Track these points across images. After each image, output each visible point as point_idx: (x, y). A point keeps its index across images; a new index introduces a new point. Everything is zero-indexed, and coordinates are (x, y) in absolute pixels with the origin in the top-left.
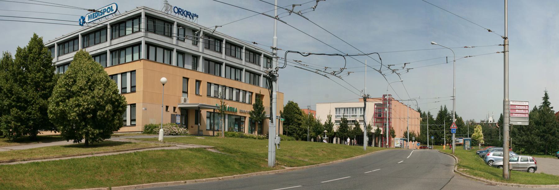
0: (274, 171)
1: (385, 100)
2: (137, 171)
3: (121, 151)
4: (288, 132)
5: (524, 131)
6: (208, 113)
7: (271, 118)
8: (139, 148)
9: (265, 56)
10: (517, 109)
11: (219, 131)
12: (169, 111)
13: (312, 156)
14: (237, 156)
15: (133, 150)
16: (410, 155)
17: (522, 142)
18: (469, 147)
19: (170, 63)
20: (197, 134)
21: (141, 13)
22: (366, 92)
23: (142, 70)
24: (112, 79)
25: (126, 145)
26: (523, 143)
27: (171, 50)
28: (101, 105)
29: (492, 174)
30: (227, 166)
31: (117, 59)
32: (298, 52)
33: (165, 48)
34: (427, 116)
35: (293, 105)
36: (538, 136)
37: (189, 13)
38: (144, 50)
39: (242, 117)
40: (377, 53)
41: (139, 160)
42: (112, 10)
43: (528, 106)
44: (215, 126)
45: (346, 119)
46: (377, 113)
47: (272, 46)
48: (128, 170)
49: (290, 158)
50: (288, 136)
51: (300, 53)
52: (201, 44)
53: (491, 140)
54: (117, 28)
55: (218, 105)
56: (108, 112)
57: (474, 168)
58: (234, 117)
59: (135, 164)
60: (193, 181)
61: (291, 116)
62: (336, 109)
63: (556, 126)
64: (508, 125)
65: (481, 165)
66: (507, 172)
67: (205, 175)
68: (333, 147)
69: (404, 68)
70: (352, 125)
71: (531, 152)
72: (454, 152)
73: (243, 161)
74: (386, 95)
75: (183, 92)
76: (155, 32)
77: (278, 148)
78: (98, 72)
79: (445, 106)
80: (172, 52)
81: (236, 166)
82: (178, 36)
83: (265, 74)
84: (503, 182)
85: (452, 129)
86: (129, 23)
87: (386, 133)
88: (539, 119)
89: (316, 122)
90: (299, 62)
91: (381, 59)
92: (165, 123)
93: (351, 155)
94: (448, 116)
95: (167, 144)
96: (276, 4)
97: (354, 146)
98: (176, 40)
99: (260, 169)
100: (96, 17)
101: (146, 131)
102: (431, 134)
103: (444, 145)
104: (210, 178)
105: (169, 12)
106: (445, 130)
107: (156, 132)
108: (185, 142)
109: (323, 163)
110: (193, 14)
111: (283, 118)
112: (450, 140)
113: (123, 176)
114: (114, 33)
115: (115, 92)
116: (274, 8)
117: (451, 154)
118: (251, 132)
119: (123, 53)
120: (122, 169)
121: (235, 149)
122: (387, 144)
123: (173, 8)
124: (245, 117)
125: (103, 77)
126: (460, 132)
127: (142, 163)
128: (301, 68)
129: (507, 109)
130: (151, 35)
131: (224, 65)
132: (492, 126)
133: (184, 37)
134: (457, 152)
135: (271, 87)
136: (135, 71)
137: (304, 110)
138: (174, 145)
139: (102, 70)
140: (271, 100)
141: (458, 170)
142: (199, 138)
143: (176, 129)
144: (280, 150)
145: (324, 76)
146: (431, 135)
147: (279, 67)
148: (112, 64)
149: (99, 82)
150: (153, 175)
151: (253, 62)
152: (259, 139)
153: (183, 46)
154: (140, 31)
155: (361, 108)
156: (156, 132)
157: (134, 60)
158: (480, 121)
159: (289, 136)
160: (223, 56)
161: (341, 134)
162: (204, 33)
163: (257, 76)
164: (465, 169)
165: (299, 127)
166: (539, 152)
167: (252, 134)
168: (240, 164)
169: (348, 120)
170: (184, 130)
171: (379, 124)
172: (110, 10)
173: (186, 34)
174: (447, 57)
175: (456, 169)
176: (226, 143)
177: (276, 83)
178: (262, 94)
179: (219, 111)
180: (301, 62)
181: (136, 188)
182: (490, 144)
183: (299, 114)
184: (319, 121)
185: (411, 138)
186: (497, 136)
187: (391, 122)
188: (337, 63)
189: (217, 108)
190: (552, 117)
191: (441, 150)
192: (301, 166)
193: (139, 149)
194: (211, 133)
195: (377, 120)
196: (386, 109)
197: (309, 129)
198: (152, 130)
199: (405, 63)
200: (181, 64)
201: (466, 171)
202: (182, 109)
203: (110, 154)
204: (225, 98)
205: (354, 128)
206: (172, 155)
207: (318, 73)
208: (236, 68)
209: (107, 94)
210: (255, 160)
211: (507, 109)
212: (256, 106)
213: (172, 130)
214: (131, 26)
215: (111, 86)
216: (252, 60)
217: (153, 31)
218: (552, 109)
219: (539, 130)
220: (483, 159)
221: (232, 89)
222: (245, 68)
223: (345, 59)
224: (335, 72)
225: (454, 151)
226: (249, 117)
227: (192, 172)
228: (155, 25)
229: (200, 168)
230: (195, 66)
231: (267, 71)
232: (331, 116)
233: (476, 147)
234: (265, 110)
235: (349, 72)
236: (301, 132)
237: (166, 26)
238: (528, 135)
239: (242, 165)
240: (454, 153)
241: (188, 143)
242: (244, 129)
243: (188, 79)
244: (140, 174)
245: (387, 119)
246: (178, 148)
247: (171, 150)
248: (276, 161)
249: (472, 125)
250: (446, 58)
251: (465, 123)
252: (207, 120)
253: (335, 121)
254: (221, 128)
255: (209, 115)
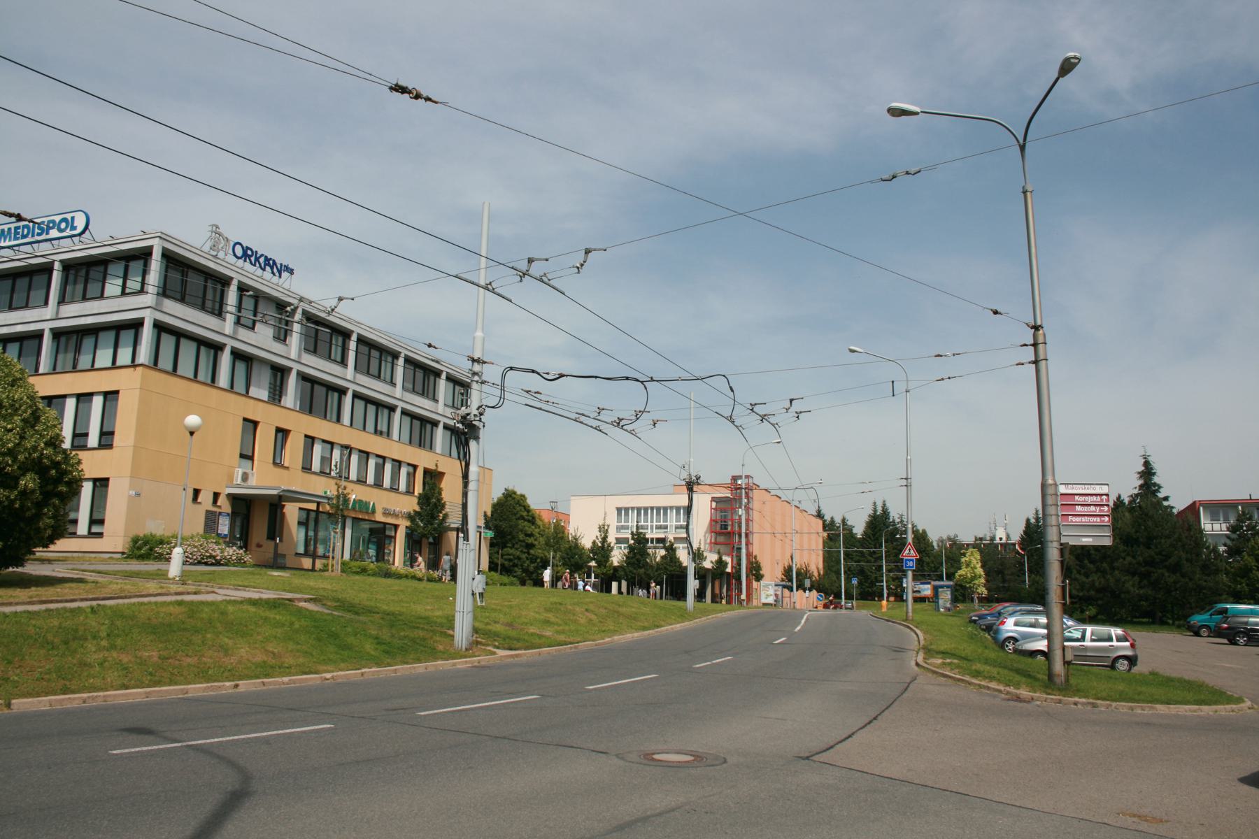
0: (468, 659)
1: (739, 488)
2: (93, 658)
3: (52, 602)
4: (503, 565)
5: (1092, 562)
6: (302, 511)
7: (463, 529)
8: (105, 595)
9: (450, 378)
10: (1078, 505)
11: (329, 557)
12: (200, 503)
13: (560, 625)
14: (372, 622)
15: (86, 600)
16: (800, 622)
17: (1088, 591)
18: (948, 605)
19: (213, 379)
20: (271, 565)
21: (151, 247)
22: (692, 471)
23: (137, 392)
24: (49, 405)
25: (67, 585)
26: (1092, 593)
27: (217, 348)
28: (7, 473)
29: (1018, 671)
30: (345, 645)
31: (70, 356)
32: (533, 371)
33: (201, 342)
34: (840, 527)
35: (514, 498)
36: (1133, 574)
37: (271, 262)
38: (147, 342)
39: (387, 526)
40: (724, 376)
41: (103, 628)
42: (74, 228)
43: (1107, 495)
44: (318, 545)
45: (644, 535)
46: (716, 521)
47: (472, 356)
48: (66, 653)
49: (507, 628)
50: (501, 574)
51: (538, 374)
52: (295, 340)
53: (1004, 587)
54: (83, 273)
55: (328, 493)
56: (24, 494)
57: (971, 658)
58: (366, 526)
59: (89, 638)
60: (255, 683)
61: (511, 527)
62: (619, 510)
63: (1183, 546)
64: (1056, 545)
65: (987, 651)
66: (1058, 667)
67: (288, 668)
68: (613, 603)
69: (790, 410)
70: (657, 551)
71: (1116, 618)
72: (911, 618)
73: (385, 634)
74: (740, 477)
75: (242, 456)
76: (182, 300)
77: (479, 604)
78: (8, 384)
79: (884, 501)
80: (219, 352)
81: (369, 647)
82: (239, 311)
83: (451, 423)
84: (1049, 694)
85: (905, 558)
86: (117, 269)
87: (740, 569)
88: (1134, 530)
89: (569, 541)
90: (536, 395)
91: (734, 389)
92: (187, 533)
93: (656, 623)
94: (891, 527)
95: (191, 588)
96: (484, 253)
97: (661, 601)
98: (233, 324)
99: (434, 654)
100: (24, 237)
101: (136, 551)
102: (850, 573)
103: (883, 600)
104: (302, 675)
105: (221, 255)
106: (886, 562)
107: (161, 554)
108: (240, 583)
109: (589, 641)
110: (281, 264)
111: (490, 529)
112: (897, 587)
113: (50, 669)
114: (69, 288)
115: (55, 442)
116: (479, 264)
117: (903, 621)
118: (409, 563)
119: (88, 342)
120: (49, 650)
121: (368, 603)
122: (743, 597)
123: (232, 244)
124: (396, 527)
125: (21, 399)
126: (922, 566)
127: (108, 635)
128: (540, 409)
129: (1051, 505)
130: (170, 305)
131: (350, 395)
132: (1005, 550)
133: (255, 315)
134: (917, 617)
135: (465, 458)
136: (117, 392)
137: (540, 512)
138: (209, 589)
139: (21, 379)
140: (466, 485)
141: (926, 663)
142: (276, 573)
143: (218, 550)
144: (482, 607)
145: (596, 429)
146: (849, 575)
147: (486, 406)
148: (54, 369)
149: (9, 411)
150: (149, 669)
151: (421, 392)
152: (430, 580)
153: (249, 342)
154: (142, 291)
155: (678, 509)
156: (162, 555)
157: (119, 363)
158: (974, 540)
159: (504, 575)
160: (350, 372)
161: (630, 572)
162: (305, 313)
163: (429, 427)
164: (948, 661)
165: (529, 553)
166: (1136, 617)
167: (412, 567)
168: (378, 641)
169: (647, 536)
170: (237, 554)
171: (723, 548)
172: (67, 227)
173: (260, 309)
174: (893, 382)
175: (920, 659)
176: (344, 588)
177: (478, 443)
178: (440, 469)
179: (332, 507)
180: (541, 394)
181: (84, 702)
182: (1001, 596)
183: (529, 521)
184: (576, 539)
185: (800, 581)
186: (1018, 576)
187: (751, 542)
188: (625, 399)
189: (326, 501)
190: (1169, 524)
191: (875, 611)
192: (535, 648)
193: (104, 599)
194: (307, 563)
195: (718, 537)
196: (740, 512)
197: (553, 558)
198: (151, 549)
199: (791, 398)
200: (240, 385)
201: (950, 664)
202: (234, 498)
203: (20, 608)
204: (348, 478)
205: (662, 557)
206: (204, 615)
207: (581, 422)
208: (378, 404)
209: (29, 446)
210: (421, 633)
211: (1051, 505)
212: (424, 499)
213: (207, 551)
214: (121, 274)
215: (45, 424)
216: (419, 387)
217: (178, 296)
218: (1165, 503)
219: (1134, 557)
220: (989, 635)
221: (365, 455)
222: (401, 405)
223: (646, 388)
224: (621, 420)
225: (910, 614)
226: (407, 527)
227: (254, 661)
228: (186, 281)
229: (276, 651)
230: (277, 392)
231: (458, 414)
232: (608, 526)
233: (968, 605)
234: (447, 509)
235: (655, 419)
236: (533, 565)
237: (210, 285)
238: (1104, 572)
239: (384, 644)
240: (912, 620)
241: (247, 587)
242: (392, 555)
243: (255, 424)
244: (101, 664)
245: (743, 535)
246: (219, 598)
247: (202, 603)
248: (473, 635)
249: (955, 551)
250: (891, 383)
251: (935, 544)
252: (298, 530)
253: (617, 539)
254: (333, 550)
255: (305, 516)
